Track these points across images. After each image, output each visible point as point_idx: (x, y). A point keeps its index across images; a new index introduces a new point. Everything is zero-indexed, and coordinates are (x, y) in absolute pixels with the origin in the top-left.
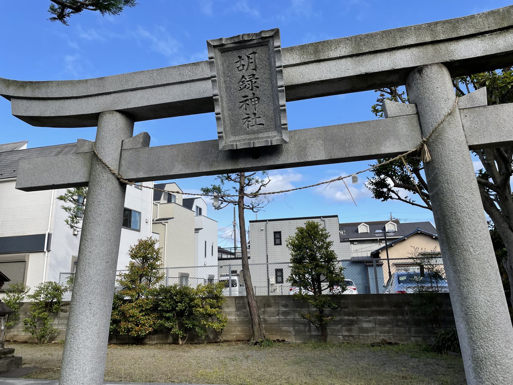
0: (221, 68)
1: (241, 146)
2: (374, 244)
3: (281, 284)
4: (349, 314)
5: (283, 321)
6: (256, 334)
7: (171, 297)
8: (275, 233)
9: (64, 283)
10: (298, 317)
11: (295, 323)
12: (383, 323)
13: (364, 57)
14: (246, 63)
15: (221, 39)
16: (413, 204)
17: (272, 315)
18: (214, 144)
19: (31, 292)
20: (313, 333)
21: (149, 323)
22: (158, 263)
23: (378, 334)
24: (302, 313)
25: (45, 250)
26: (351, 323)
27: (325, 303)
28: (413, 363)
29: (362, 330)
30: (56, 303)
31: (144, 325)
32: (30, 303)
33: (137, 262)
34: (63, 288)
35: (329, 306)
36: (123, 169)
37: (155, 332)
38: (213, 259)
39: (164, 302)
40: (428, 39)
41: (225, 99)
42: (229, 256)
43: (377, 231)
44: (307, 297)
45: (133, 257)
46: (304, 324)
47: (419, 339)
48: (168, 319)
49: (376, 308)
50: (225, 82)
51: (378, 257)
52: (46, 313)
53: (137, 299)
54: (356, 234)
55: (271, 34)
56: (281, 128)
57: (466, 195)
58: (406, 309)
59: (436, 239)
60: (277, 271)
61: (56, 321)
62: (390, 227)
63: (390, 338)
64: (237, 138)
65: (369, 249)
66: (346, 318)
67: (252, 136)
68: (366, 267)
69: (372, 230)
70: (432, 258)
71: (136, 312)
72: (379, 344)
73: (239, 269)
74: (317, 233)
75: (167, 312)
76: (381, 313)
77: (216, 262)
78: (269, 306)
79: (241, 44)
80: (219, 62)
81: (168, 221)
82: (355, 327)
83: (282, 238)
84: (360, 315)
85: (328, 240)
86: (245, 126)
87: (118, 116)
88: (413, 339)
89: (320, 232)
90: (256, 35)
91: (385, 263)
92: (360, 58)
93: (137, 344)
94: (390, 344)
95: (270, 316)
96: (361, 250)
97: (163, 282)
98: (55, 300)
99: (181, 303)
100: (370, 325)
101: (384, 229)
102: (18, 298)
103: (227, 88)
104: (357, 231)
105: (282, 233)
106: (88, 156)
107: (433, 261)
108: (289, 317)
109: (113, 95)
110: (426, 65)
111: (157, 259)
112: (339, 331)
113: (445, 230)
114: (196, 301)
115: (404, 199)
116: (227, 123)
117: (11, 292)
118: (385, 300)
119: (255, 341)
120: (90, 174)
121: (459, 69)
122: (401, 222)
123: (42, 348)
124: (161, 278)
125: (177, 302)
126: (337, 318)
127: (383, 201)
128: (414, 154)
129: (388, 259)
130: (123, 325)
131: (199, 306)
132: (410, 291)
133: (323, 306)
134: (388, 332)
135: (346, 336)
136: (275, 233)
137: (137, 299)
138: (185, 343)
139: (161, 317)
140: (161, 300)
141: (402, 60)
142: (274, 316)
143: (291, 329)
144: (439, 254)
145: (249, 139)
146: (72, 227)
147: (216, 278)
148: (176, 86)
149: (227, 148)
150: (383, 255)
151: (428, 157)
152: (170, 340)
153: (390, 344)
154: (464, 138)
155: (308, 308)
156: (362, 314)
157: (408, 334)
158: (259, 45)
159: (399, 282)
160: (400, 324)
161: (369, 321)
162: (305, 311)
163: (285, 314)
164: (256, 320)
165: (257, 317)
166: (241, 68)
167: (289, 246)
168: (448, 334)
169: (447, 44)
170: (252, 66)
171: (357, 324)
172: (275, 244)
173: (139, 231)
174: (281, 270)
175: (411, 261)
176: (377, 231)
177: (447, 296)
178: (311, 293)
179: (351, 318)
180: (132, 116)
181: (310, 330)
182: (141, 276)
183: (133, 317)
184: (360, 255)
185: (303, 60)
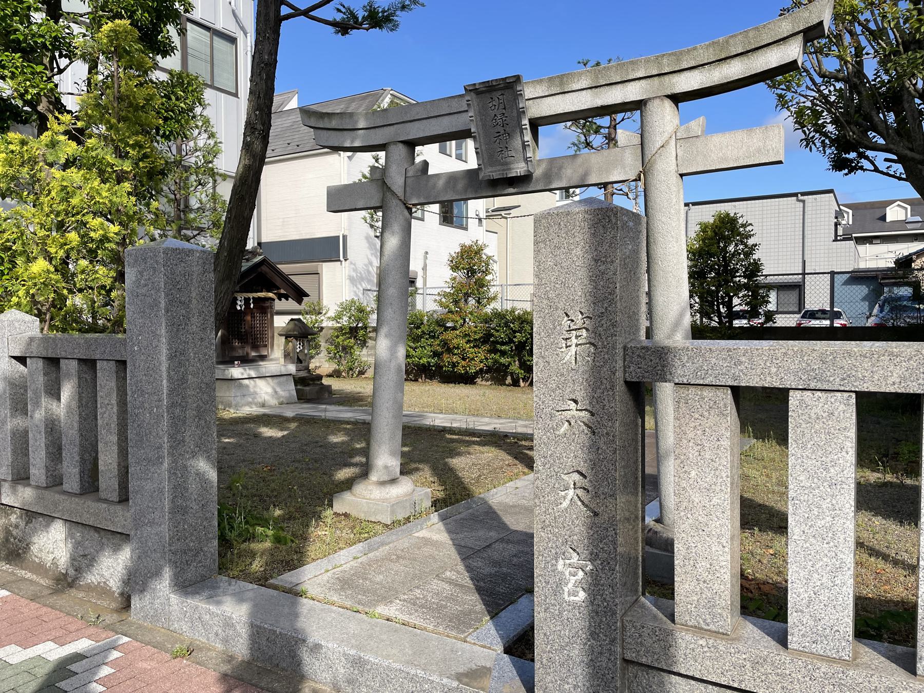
7: (506, 325)
9: (370, 302)
13: (602, 88)
15: (475, 84)
19: (331, 314)
21: (479, 358)
22: (488, 278)
25: (341, 258)
30: (362, 328)
31: (473, 359)
32: (331, 328)
33: (460, 275)
34: (369, 309)
36: (408, 194)
37: (489, 370)
39: (498, 331)
40: (655, 72)
45: (455, 268)
48: (503, 353)
52: (352, 341)
53: (462, 326)
54: (880, 223)
55: (514, 79)
57: (664, 219)
61: (365, 351)
64: (494, 169)
71: (462, 342)
75: (503, 344)
85: (751, 242)
86: (500, 158)
87: (401, 146)
92: (598, 90)
93: (466, 384)
97: (493, 305)
98: (360, 325)
102: (316, 320)
103: (483, 125)
104: (883, 218)
106: (380, 183)
110: (650, 99)
111: (486, 272)
115: (885, 171)
116: (485, 156)
117: (307, 314)
120: (383, 200)
123: (352, 382)
124: (494, 298)
125: (515, 332)
127: (846, 174)
130: (446, 358)
137: (462, 326)
139: (494, 351)
140: (493, 329)
141: (632, 92)
146: (372, 226)
148: (446, 117)
152: (509, 380)
169: (670, 76)
170: (502, 106)
173: (466, 229)
182: (467, 295)
183: (458, 348)
184: (872, 265)
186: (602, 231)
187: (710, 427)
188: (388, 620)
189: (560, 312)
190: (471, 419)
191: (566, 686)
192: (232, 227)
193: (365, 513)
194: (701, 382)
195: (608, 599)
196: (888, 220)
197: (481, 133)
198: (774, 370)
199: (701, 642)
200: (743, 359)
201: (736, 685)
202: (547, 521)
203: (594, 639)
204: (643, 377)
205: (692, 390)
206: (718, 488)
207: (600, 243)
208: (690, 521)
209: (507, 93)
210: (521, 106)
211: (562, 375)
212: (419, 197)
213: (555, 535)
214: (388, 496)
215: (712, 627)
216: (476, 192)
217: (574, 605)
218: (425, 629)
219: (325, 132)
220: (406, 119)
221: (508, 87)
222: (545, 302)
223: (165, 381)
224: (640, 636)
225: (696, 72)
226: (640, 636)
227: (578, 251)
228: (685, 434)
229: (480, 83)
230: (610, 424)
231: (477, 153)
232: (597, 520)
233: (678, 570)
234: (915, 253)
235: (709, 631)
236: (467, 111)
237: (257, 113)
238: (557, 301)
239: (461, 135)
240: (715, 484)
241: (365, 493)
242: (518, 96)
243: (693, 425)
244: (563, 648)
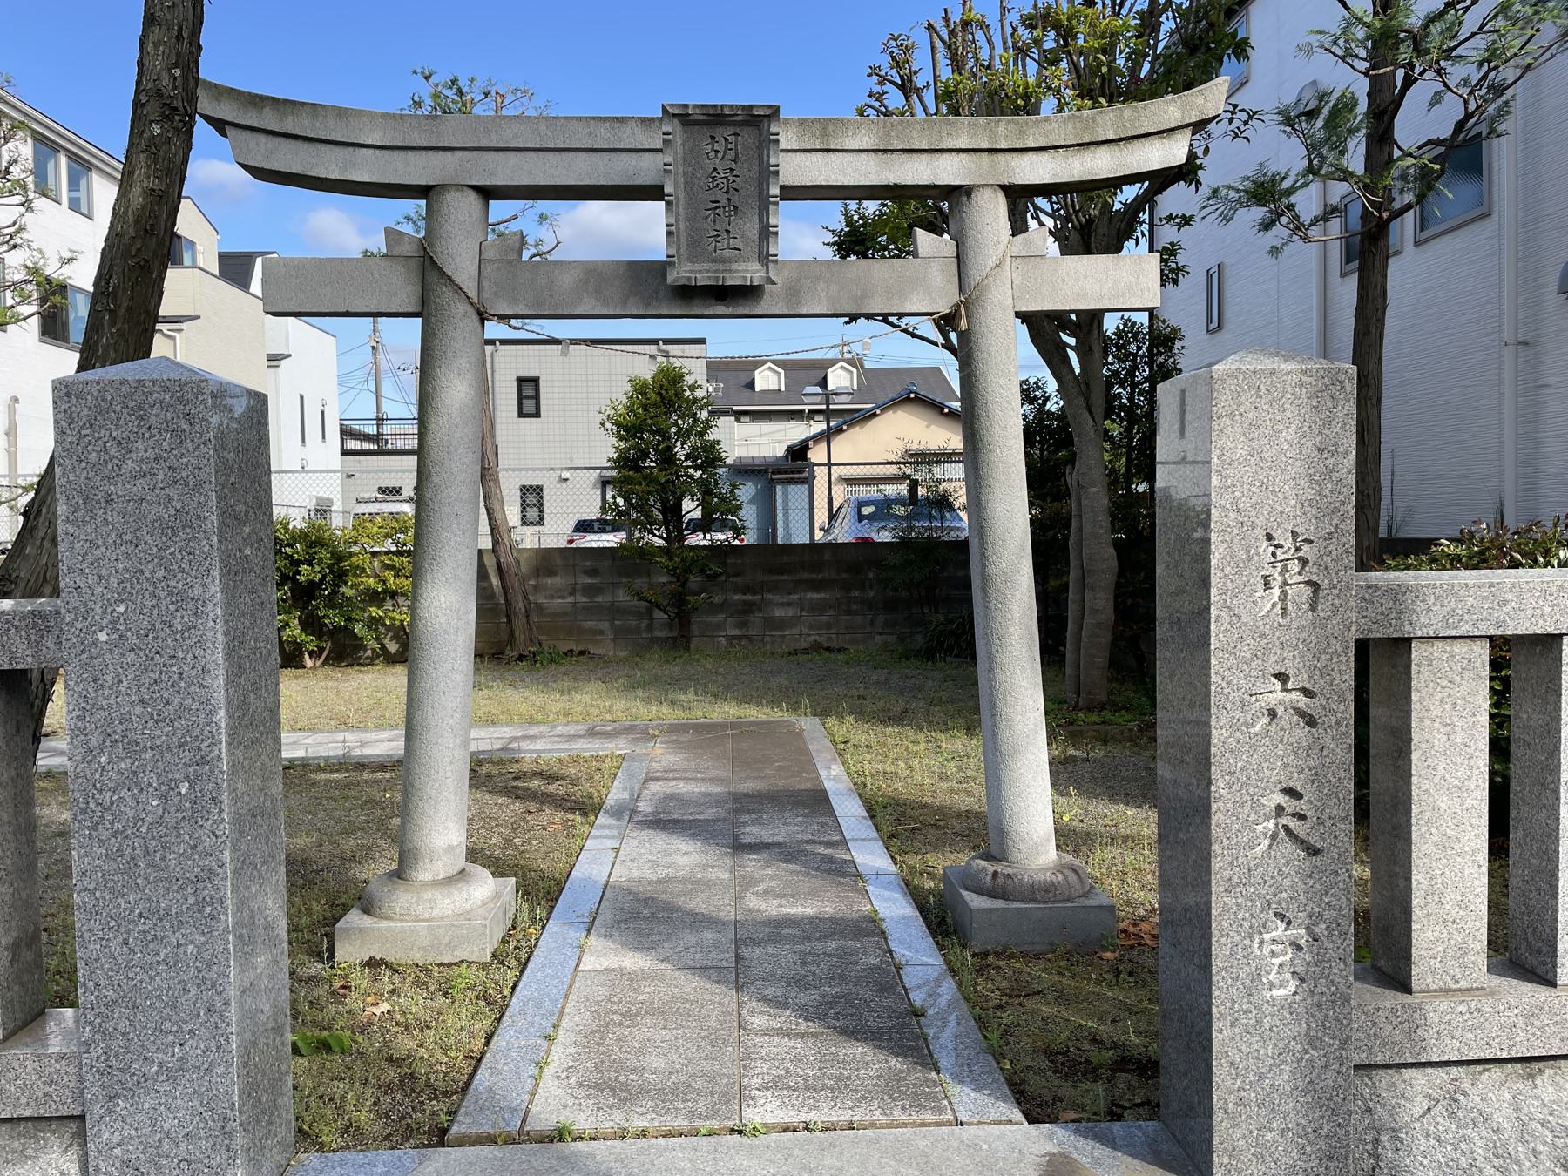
0: (680, 150)
1: (702, 280)
2: (793, 424)
3: (537, 528)
4: (746, 589)
5: (584, 608)
6: (520, 637)
8: (521, 381)
10: (622, 597)
11: (614, 611)
12: (819, 608)
13: (895, 156)
14: (721, 150)
15: (686, 106)
16: (913, 335)
17: (559, 593)
18: (660, 269)
20: (658, 634)
23: (805, 631)
24: (636, 587)
26: (748, 608)
27: (693, 562)
28: (881, 675)
29: (772, 624)
35: (702, 571)
36: (486, 295)
38: (327, 453)
40: (985, 145)
41: (682, 202)
42: (367, 446)
43: (809, 389)
44: (646, 553)
46: (638, 614)
47: (890, 639)
49: (806, 576)
50: (685, 173)
51: (805, 458)
54: (747, 392)
56: (766, 258)
57: (1002, 381)
58: (871, 575)
59: (952, 414)
60: (525, 490)
62: (838, 378)
63: (830, 639)
64: (697, 267)
65: (779, 436)
66: (737, 597)
67: (721, 267)
68: (772, 484)
69: (794, 389)
70: (938, 462)
72: (805, 651)
73: (408, 485)
74: (679, 394)
76: (817, 586)
77: (336, 460)
78: (551, 572)
79: (714, 119)
80: (679, 141)
81: (183, 326)
82: (756, 618)
83: (542, 396)
84: (769, 591)
88: (877, 638)
89: (687, 393)
90: (743, 107)
91: (821, 473)
92: (888, 155)
94: (828, 649)
95: (552, 597)
96: (758, 440)
99: (310, 564)
100: (790, 612)
101: (823, 383)
103: (686, 183)
105: (542, 383)
106: (413, 264)
107: (938, 471)
108: (599, 599)
109: (459, 154)
112: (718, 627)
113: (973, 454)
114: (354, 559)
116: (683, 240)
118: (827, 556)
119: (516, 654)
121: (1019, 197)
122: (868, 365)
125: (298, 563)
126: (718, 599)
128: (945, 317)
129: (829, 465)
131: (364, 570)
132: (885, 537)
133: (687, 570)
134: (828, 626)
135: (734, 637)
136: (521, 381)
138: (323, 664)
142: (562, 597)
143: (605, 625)
144: (954, 453)
145: (716, 271)
147: (337, 507)
149: (680, 283)
150: (817, 454)
151: (963, 325)
153: (828, 649)
154: (1010, 301)
155: (649, 575)
156: (774, 588)
157: (869, 629)
158: (745, 124)
159: (861, 518)
160: (854, 607)
161: (789, 604)
162: (640, 583)
163: (590, 591)
164: (520, 606)
165: (520, 598)
166: (712, 155)
167: (608, 425)
168: (951, 622)
169: (1008, 155)
171: (760, 610)
172: (521, 415)
174: (538, 490)
175: (892, 470)
176: (809, 389)
177: (963, 546)
178: (658, 542)
179: (748, 597)
180: (487, 193)
181: (650, 628)
185: (803, 146)
186: (1329, 404)
187: (1463, 697)
188: (785, 1130)
189: (1261, 534)
190: (352, 738)
191: (1269, 1136)
192: (121, 334)
193: (424, 949)
194: (1453, 633)
195: (1337, 980)
196: (757, 389)
197: (681, 196)
198: (1547, 610)
199: (1463, 1008)
200: (1509, 597)
201: (1505, 1055)
202: (1236, 879)
203: (1315, 1048)
204: (1370, 631)
205: (1438, 644)
206: (1473, 785)
207: (1327, 423)
208: (1435, 838)
209: (747, 137)
210: (772, 161)
211: (1262, 636)
212: (514, 301)
213: (1249, 898)
214: (467, 906)
215: (1464, 984)
216: (647, 305)
217: (1282, 1005)
218: (873, 1125)
219: (262, 138)
220: (485, 143)
221: (754, 123)
222: (1232, 515)
223: (222, 713)
224: (1374, 1024)
225: (1044, 157)
226: (1374, 1024)
227: (1290, 434)
228: (1428, 711)
229: (695, 106)
230: (1342, 707)
231: (669, 234)
232: (1318, 861)
233: (1417, 913)
234: (812, 438)
235: (1460, 990)
236: (660, 150)
237: (177, 72)
238: (1253, 513)
239: (651, 192)
240: (1469, 779)
241: (420, 909)
242: (768, 142)
243: (1439, 696)
244: (1262, 1076)
